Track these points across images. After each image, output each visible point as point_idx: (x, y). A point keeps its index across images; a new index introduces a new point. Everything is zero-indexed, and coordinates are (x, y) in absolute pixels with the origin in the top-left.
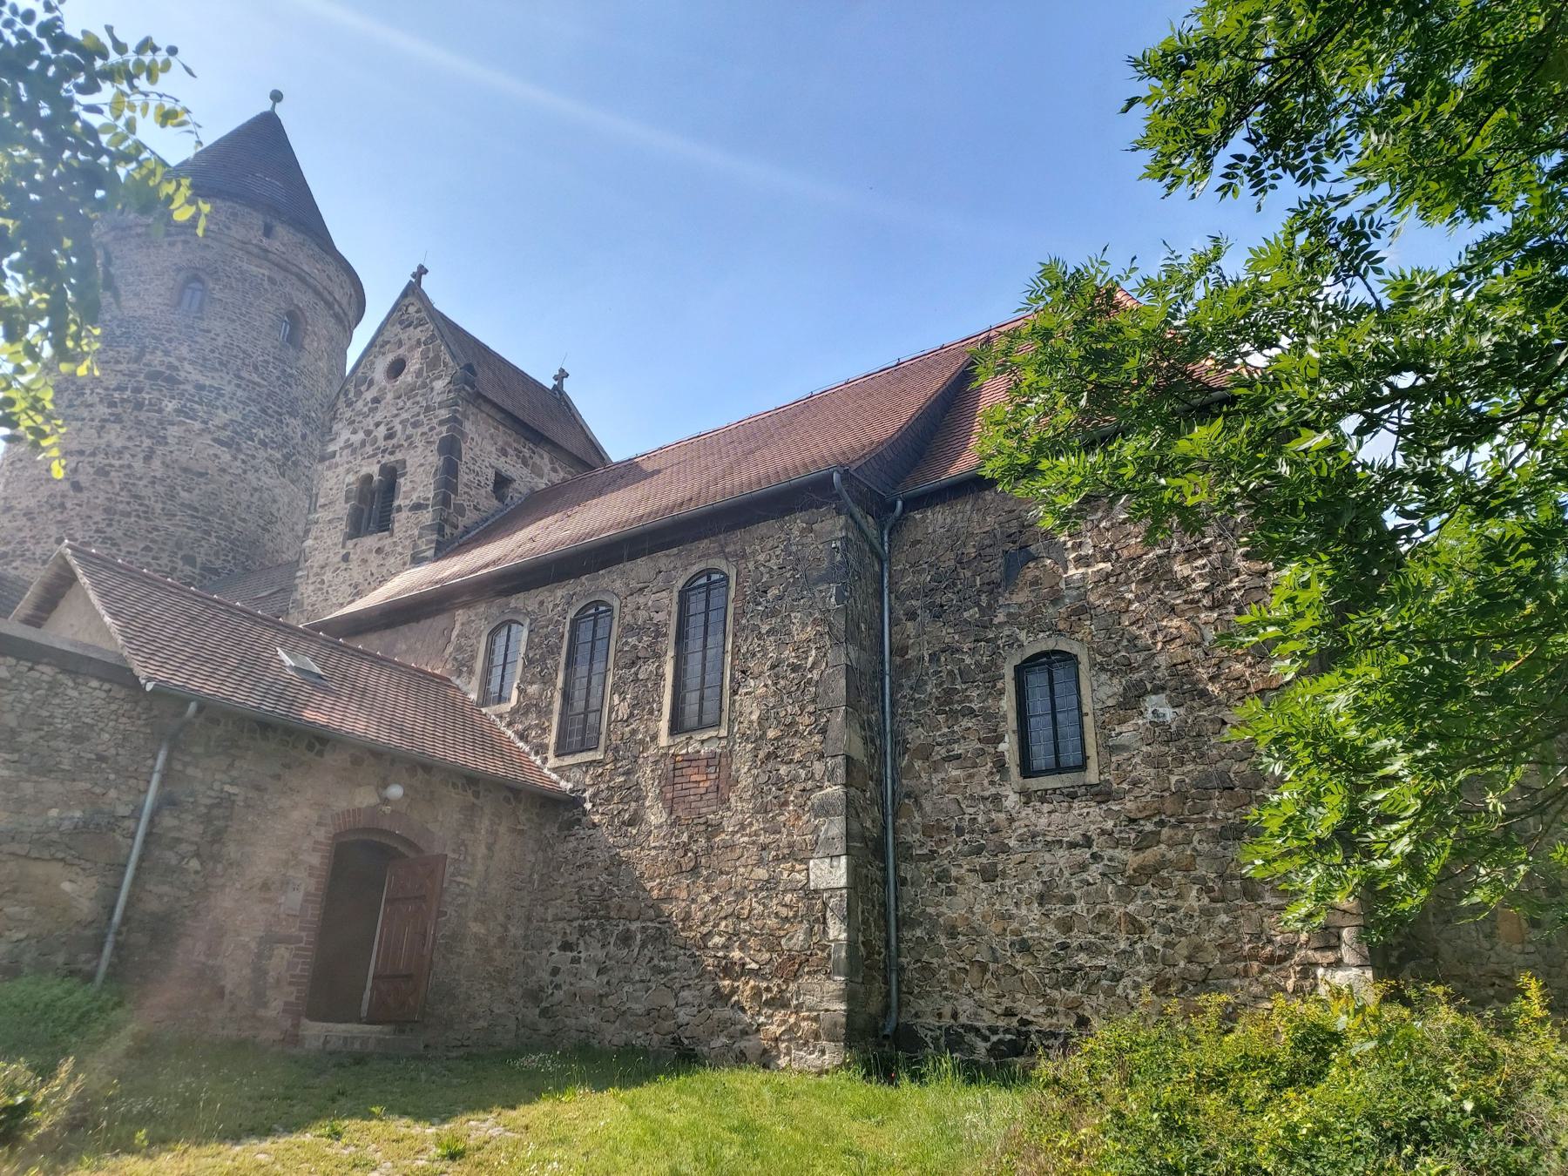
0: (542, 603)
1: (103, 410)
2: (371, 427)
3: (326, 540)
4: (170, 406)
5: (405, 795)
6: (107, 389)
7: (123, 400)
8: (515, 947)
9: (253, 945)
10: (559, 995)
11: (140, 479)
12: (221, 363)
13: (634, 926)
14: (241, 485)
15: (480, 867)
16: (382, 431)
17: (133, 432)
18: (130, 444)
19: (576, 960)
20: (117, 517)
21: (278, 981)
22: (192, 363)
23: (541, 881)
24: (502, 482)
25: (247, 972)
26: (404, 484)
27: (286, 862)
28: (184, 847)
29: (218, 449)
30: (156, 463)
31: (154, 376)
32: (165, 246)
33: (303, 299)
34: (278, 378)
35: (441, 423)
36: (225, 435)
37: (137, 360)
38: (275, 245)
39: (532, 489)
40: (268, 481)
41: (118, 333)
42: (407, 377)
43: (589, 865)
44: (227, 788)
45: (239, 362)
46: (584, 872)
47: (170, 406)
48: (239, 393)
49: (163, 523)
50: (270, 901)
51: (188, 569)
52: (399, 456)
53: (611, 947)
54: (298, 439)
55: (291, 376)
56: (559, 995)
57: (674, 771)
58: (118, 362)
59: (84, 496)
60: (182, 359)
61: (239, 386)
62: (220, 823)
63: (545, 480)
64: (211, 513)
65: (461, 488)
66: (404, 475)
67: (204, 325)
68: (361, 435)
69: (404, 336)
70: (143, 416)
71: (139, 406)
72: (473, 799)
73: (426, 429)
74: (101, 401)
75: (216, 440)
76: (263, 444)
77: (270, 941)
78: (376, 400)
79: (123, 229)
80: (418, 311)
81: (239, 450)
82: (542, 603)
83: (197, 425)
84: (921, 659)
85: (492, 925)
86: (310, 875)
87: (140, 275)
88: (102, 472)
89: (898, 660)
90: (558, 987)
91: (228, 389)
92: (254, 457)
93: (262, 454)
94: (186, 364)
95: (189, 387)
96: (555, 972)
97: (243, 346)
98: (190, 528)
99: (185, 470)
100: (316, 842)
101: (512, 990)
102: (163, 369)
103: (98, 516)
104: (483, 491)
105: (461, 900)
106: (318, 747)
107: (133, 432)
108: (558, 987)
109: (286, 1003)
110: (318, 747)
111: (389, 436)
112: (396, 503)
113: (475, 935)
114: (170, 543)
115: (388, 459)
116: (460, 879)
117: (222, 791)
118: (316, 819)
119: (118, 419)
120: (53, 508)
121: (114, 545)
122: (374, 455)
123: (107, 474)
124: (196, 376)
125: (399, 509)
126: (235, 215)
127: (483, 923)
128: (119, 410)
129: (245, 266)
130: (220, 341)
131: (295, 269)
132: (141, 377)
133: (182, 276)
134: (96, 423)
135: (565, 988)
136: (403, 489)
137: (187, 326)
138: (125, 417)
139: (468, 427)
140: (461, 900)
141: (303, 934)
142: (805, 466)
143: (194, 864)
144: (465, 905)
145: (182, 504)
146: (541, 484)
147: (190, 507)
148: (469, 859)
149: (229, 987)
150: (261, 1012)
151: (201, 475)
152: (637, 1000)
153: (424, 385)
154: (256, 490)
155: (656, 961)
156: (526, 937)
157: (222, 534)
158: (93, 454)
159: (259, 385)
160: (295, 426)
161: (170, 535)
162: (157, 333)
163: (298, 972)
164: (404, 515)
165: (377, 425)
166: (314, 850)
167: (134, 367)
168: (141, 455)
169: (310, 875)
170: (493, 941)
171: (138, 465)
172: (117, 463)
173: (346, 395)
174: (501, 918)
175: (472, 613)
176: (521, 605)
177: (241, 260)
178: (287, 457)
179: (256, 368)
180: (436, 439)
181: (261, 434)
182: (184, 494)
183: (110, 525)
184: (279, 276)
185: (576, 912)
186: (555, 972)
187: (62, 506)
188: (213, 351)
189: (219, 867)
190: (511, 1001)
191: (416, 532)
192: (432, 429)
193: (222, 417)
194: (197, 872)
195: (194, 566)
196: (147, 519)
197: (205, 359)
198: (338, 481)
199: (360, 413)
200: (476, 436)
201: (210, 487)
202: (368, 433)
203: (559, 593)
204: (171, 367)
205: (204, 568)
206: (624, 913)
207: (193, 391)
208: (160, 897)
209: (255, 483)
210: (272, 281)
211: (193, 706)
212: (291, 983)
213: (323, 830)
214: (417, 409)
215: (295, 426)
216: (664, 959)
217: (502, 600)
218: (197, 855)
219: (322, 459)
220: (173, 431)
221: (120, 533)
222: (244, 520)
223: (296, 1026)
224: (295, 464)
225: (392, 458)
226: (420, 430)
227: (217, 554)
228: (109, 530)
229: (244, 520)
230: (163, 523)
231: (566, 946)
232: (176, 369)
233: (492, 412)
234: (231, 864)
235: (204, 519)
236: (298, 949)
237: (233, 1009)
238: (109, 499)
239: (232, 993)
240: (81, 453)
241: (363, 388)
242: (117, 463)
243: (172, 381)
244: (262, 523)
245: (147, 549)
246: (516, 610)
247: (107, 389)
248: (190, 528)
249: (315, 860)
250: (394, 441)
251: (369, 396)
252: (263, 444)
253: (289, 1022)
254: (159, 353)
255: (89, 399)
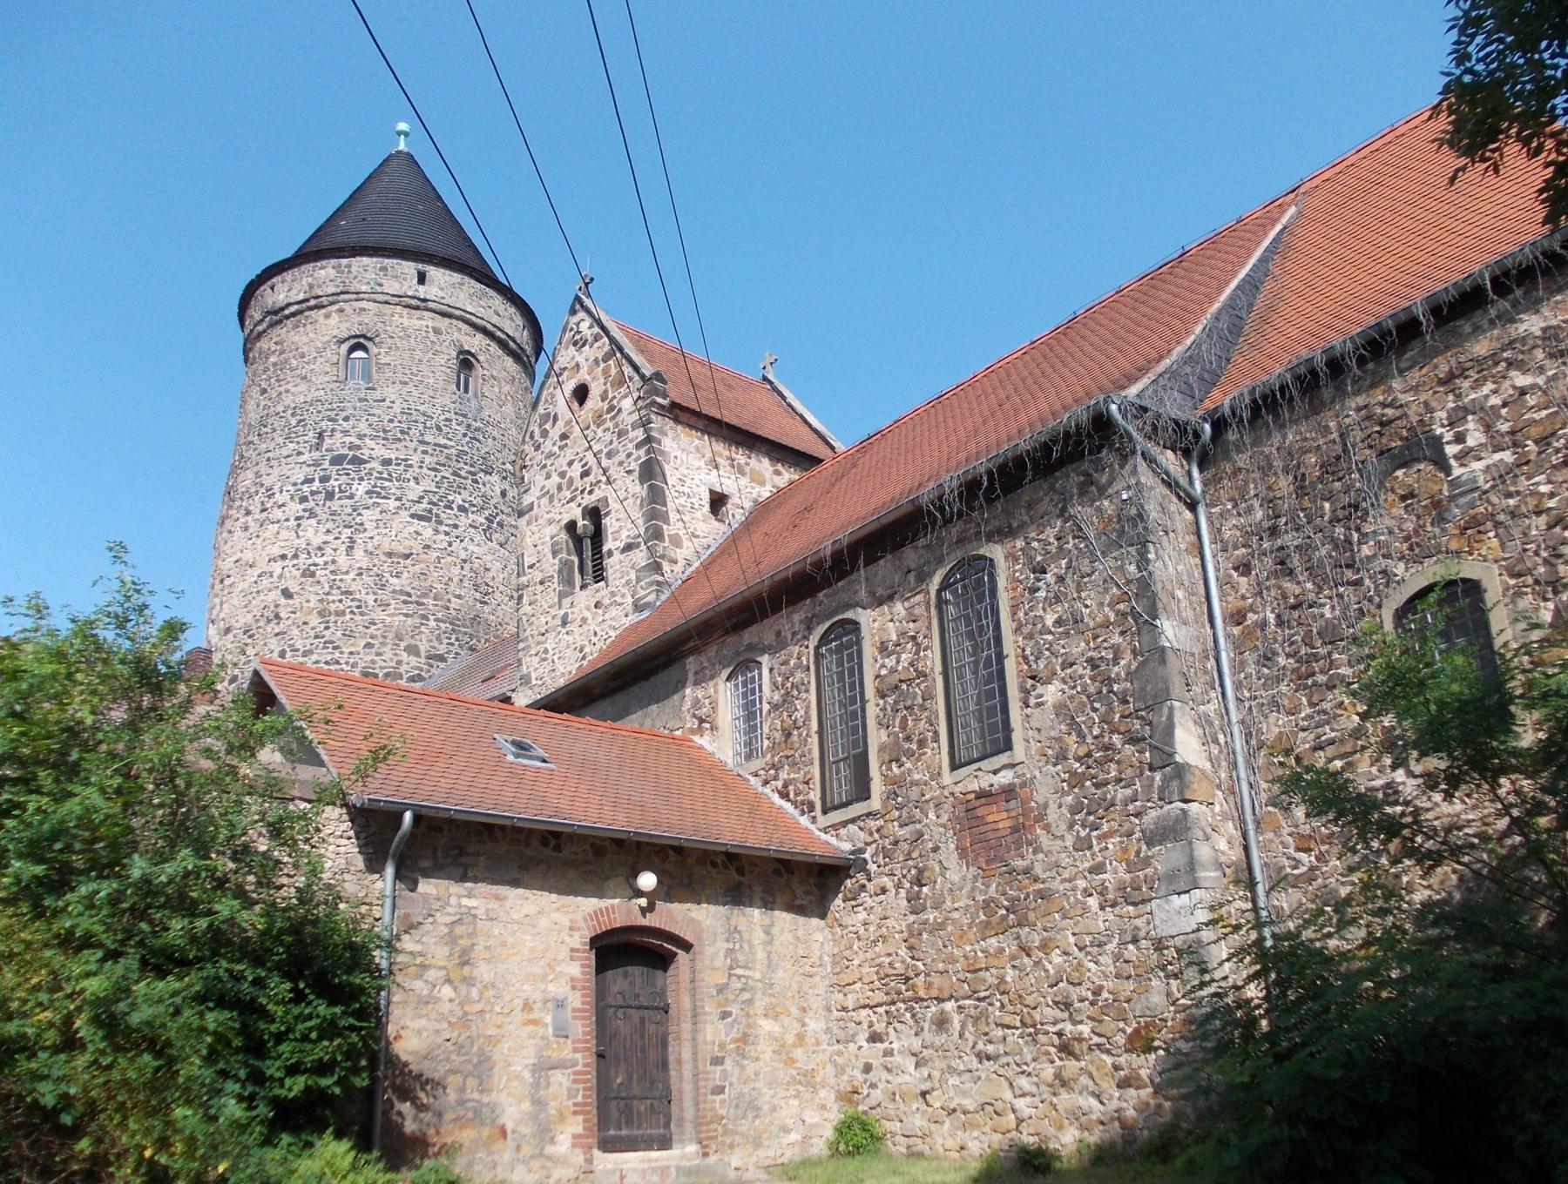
0: (778, 634)
1: (296, 508)
2: (565, 468)
3: (543, 604)
4: (360, 489)
5: (659, 882)
6: (295, 484)
7: (313, 493)
8: (818, 1043)
9: (527, 1075)
10: (877, 1095)
11: (347, 573)
12: (402, 432)
13: (950, 1006)
14: (449, 559)
15: (761, 954)
16: (577, 470)
17: (330, 525)
18: (330, 538)
19: (888, 1053)
20: (332, 618)
21: (561, 1114)
22: (373, 438)
23: (834, 963)
24: (718, 502)
25: (526, 1105)
26: (609, 523)
27: (544, 978)
28: (432, 974)
29: (418, 525)
30: (359, 553)
31: (337, 460)
32: (321, 319)
33: (475, 343)
34: (465, 435)
35: (638, 446)
36: (419, 509)
37: (318, 447)
38: (430, 291)
39: (755, 501)
40: (476, 549)
41: (294, 422)
42: (593, 402)
43: (884, 939)
44: (465, 901)
45: (421, 427)
46: (880, 948)
47: (360, 489)
48: (428, 459)
49: (379, 615)
50: (535, 1022)
51: (413, 659)
52: (598, 494)
53: (926, 1035)
54: (497, 499)
55: (477, 429)
56: (877, 1095)
57: (970, 814)
58: (300, 453)
59: (296, 602)
60: (361, 437)
61: (425, 452)
62: (463, 942)
63: (769, 487)
64: (425, 595)
65: (673, 516)
66: (607, 514)
67: (377, 395)
68: (556, 479)
69: (580, 359)
70: (335, 505)
71: (330, 496)
72: (737, 877)
73: (622, 456)
74: (292, 498)
75: (412, 516)
76: (462, 509)
77: (544, 1067)
78: (564, 437)
79: (276, 313)
80: (591, 327)
81: (440, 523)
82: (778, 634)
83: (392, 504)
84: (1263, 624)
85: (786, 1020)
86: (573, 988)
87: (303, 356)
88: (309, 573)
89: (1236, 630)
90: (873, 1086)
91: (415, 459)
92: (456, 526)
93: (464, 521)
94: (367, 440)
95: (375, 465)
96: (867, 1068)
97: (422, 408)
98: (406, 615)
99: (390, 555)
100: (572, 950)
101: (823, 1093)
102: (345, 451)
103: (315, 620)
104: (698, 515)
105: (746, 996)
106: (553, 842)
107: (330, 525)
108: (873, 1086)
109: (575, 1136)
110: (553, 842)
111: (585, 474)
112: (605, 549)
113: (770, 1034)
114: (390, 635)
115: (588, 500)
116: (739, 972)
117: (460, 906)
118: (567, 924)
119: (312, 514)
120: (269, 621)
121: (335, 648)
122: (572, 500)
123: (313, 575)
124: (381, 452)
125: (610, 553)
126: (384, 269)
127: (776, 1018)
128: (312, 504)
129: (406, 322)
130: (397, 408)
131: (458, 313)
132: (326, 464)
133: (345, 347)
134: (293, 523)
135: (881, 1086)
136: (610, 530)
137: (360, 400)
138: (318, 510)
139: (668, 444)
140: (746, 996)
141: (578, 1056)
142: (1043, 421)
143: (447, 991)
144: (750, 1002)
145: (394, 592)
146: (765, 492)
147: (402, 592)
148: (746, 946)
149: (509, 1127)
150: (550, 1149)
151: (407, 556)
152: (965, 1094)
153: (611, 408)
154: (465, 561)
155: (980, 1046)
156: (828, 1030)
157: (440, 615)
158: (296, 556)
159: (445, 447)
160: (495, 484)
161: (388, 627)
162: (332, 414)
163: (580, 1099)
164: (617, 556)
165: (570, 464)
166: (572, 959)
167: (316, 455)
168: (343, 548)
169: (573, 988)
170: (790, 1039)
171: (343, 560)
172: (320, 561)
173: (532, 437)
174: (795, 1011)
175: (703, 658)
176: (755, 640)
177: (401, 316)
178: (489, 520)
179: (439, 429)
180: (634, 466)
181: (459, 500)
182: (394, 581)
183: (327, 628)
184: (444, 323)
185: (880, 997)
186: (867, 1068)
187: (277, 616)
188: (391, 421)
189: (474, 992)
190: (823, 1107)
191: (633, 576)
192: (629, 455)
193: (414, 491)
194: (451, 1001)
195: (418, 654)
196: (362, 614)
197: (385, 431)
198: (541, 537)
199: (550, 455)
200: (679, 454)
201: (417, 569)
202: (562, 475)
203: (797, 617)
204: (352, 447)
205: (428, 657)
206: (935, 993)
207: (380, 468)
208: (419, 1032)
209: (463, 555)
210: (437, 331)
211: (408, 816)
212: (575, 1113)
213: (577, 935)
214: (608, 436)
215: (495, 484)
216: (990, 1042)
217: (731, 639)
218: (448, 981)
219: (521, 514)
220: (369, 516)
221: (339, 634)
222: (459, 597)
223: (589, 1161)
224: (501, 525)
225: (593, 498)
226: (616, 460)
227: (439, 638)
228: (327, 633)
229: (459, 597)
230: (379, 615)
231: (875, 1038)
232: (359, 447)
233: (693, 420)
234: (485, 987)
235: (418, 603)
236: (576, 1073)
237: (518, 1148)
238: (321, 601)
239: (514, 1132)
240: (284, 557)
241: (548, 426)
242: (320, 561)
243: (357, 461)
244: (478, 596)
245: (369, 645)
246: (751, 648)
247: (295, 484)
248: (406, 615)
249: (575, 969)
250: (591, 478)
251: (555, 433)
252: (462, 509)
253: (582, 1158)
254: (338, 435)
255: (279, 498)
